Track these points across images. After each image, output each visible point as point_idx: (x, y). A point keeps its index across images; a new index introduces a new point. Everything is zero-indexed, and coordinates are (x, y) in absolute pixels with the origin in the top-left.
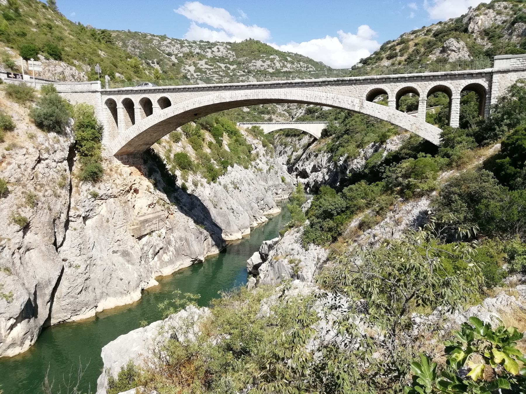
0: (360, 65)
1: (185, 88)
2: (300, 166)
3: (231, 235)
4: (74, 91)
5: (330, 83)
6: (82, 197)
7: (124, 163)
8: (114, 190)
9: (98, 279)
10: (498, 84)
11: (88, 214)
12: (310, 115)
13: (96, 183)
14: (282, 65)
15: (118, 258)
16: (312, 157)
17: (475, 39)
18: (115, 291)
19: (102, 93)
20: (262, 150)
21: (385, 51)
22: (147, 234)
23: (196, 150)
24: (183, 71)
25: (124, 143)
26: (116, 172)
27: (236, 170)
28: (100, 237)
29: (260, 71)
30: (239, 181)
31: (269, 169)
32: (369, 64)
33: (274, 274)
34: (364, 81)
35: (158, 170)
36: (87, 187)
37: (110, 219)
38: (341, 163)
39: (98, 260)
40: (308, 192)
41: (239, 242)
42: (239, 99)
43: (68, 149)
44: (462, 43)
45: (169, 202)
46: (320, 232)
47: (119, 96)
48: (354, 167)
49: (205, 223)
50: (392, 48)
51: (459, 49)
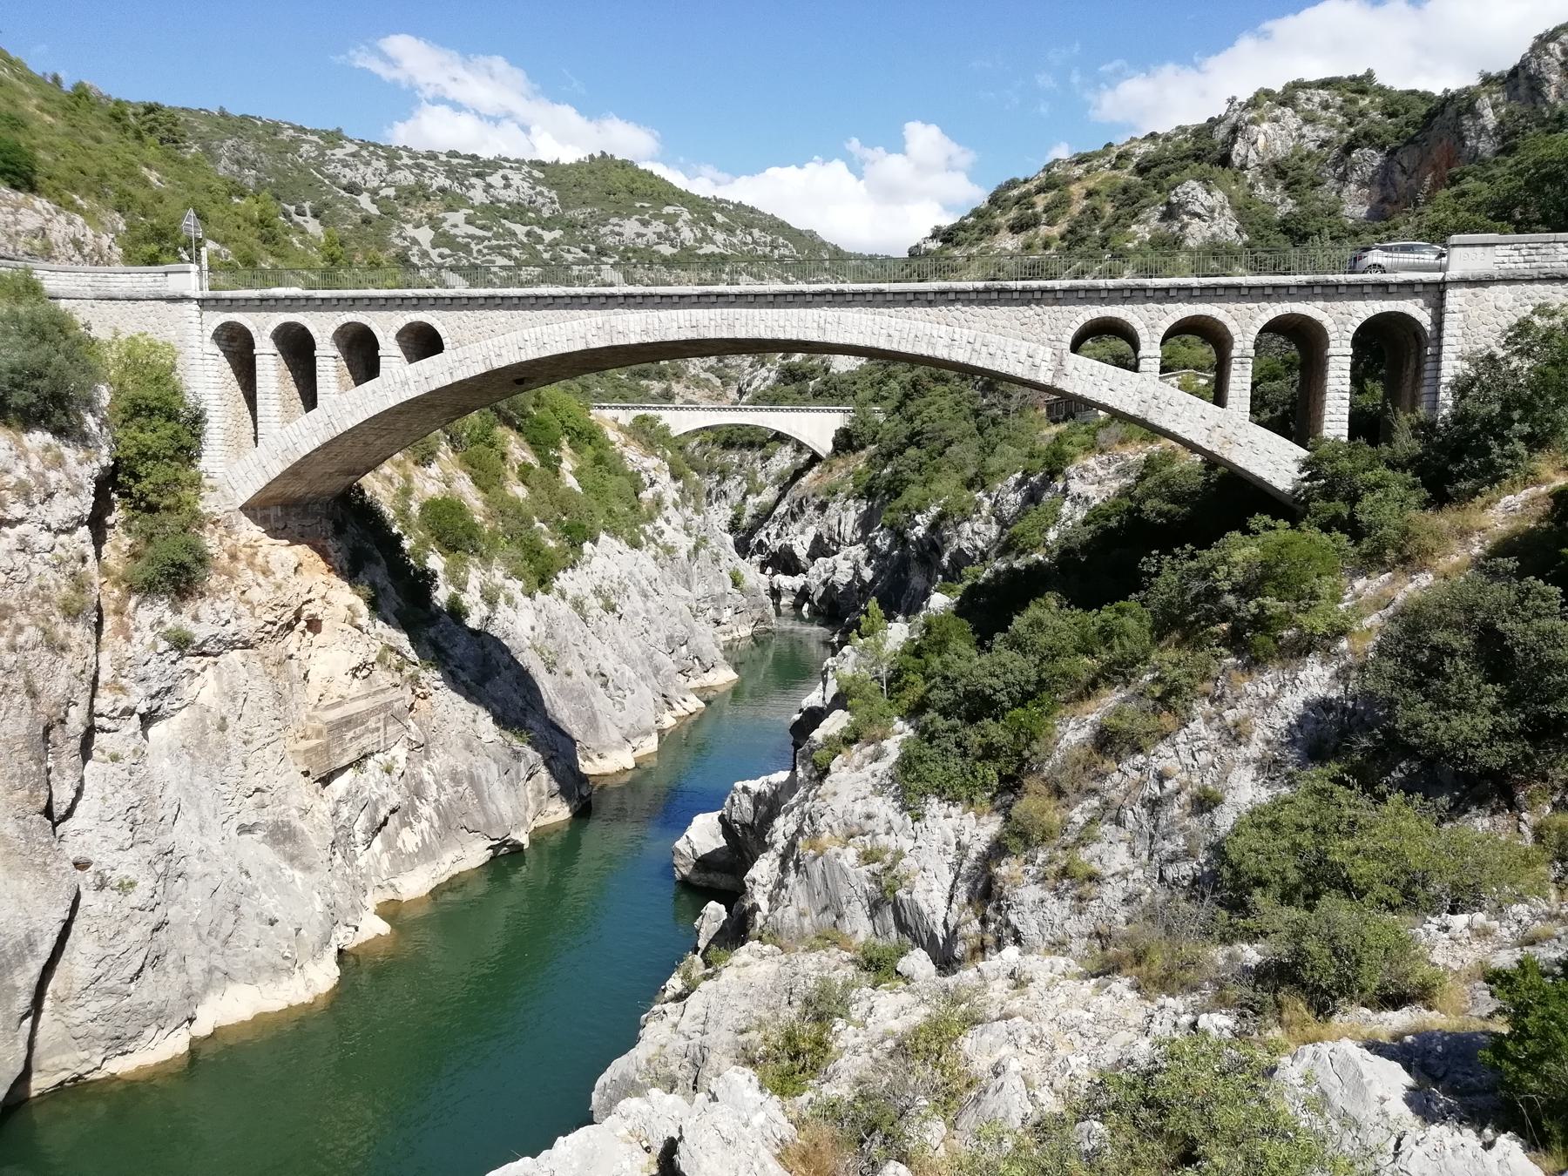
0: (934, 245)
1: (493, 297)
2: (773, 536)
3: (600, 756)
4: (101, 293)
5: (962, 296)
6: (136, 649)
7: (274, 533)
8: (243, 622)
9: (195, 925)
10: (1460, 316)
11: (156, 703)
12: (793, 387)
13: (184, 599)
14: (699, 235)
15: (255, 850)
16: (810, 511)
17: (1252, 186)
18: (253, 963)
19: (203, 303)
20: (669, 489)
21: (1005, 210)
22: (350, 765)
23: (485, 490)
24: (397, 241)
25: (277, 469)
26: (251, 565)
27: (606, 550)
28: (198, 779)
29: (635, 251)
30: (615, 586)
31: (696, 549)
32: (958, 244)
33: (811, 897)
34: (1069, 295)
35: (377, 553)
36: (155, 615)
37: (231, 720)
38: (920, 531)
39: (193, 859)
40: (806, 616)
41: (627, 778)
42: (672, 336)
43: (92, 487)
44: (1219, 195)
45: (417, 659)
46: (959, 760)
47: (264, 314)
48: (965, 544)
49: (529, 722)
50: (1024, 201)
51: (1213, 211)
